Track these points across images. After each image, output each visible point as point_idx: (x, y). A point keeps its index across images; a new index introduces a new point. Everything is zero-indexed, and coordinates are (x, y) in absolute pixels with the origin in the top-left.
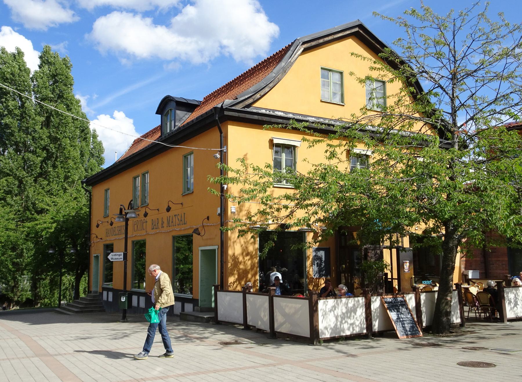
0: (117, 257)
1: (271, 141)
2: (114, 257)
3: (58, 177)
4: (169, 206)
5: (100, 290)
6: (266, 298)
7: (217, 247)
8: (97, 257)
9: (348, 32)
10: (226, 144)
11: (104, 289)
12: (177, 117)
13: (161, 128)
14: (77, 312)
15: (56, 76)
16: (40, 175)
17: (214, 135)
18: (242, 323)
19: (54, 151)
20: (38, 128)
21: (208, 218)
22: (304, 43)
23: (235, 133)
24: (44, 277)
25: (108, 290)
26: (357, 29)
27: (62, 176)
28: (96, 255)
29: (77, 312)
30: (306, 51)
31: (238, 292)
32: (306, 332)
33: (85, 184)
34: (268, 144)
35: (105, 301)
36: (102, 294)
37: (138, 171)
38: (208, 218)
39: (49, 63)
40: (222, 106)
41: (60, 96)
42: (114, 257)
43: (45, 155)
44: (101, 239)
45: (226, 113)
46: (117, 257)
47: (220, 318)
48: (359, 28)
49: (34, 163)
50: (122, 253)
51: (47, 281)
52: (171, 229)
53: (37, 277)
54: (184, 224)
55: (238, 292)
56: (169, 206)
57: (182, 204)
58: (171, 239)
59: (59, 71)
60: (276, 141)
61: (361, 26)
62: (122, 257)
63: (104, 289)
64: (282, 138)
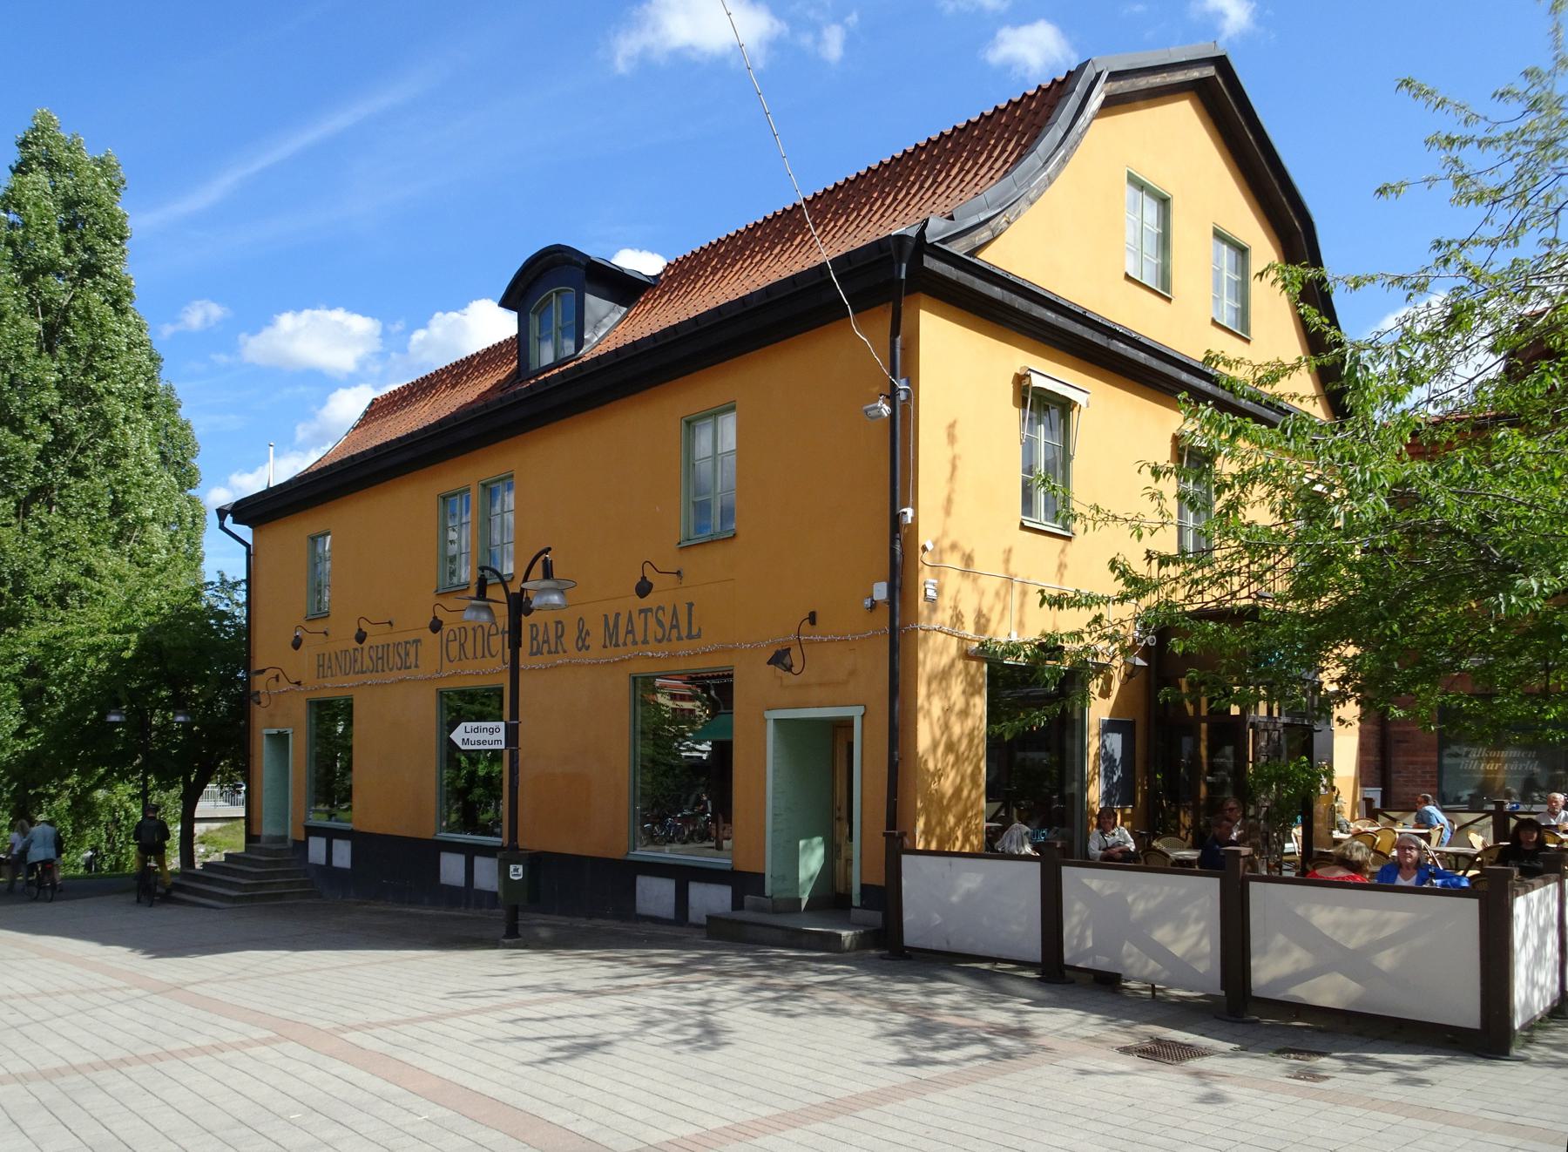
0: (485, 736)
1: (1021, 381)
2: (473, 737)
3: (93, 505)
4: (644, 578)
5: (294, 832)
6: (1205, 892)
7: (861, 710)
8: (281, 740)
9: (1179, 77)
10: (912, 377)
11: (312, 831)
12: (588, 316)
13: (519, 345)
14: (234, 899)
15: (78, 203)
16: (36, 494)
17: (863, 337)
18: (1037, 956)
19: (75, 426)
20: (29, 351)
21: (812, 618)
22: (1114, 76)
23: (941, 339)
24: (52, 791)
25: (330, 835)
26: (1210, 71)
27: (106, 502)
28: (274, 731)
29: (234, 899)
30: (1113, 104)
31: (1027, 858)
32: (1466, 1011)
33: (229, 518)
34: (1009, 390)
35: (318, 866)
36: (302, 847)
37: (467, 474)
38: (812, 618)
39: (52, 165)
40: (921, 234)
41: (89, 270)
42: (473, 737)
43: (50, 438)
44: (298, 683)
45: (930, 263)
46: (485, 736)
47: (911, 937)
48: (1219, 69)
49: (18, 459)
50: (502, 725)
51: (64, 802)
52: (622, 652)
53: (31, 792)
54: (690, 637)
55: (1027, 858)
56: (644, 578)
57: (678, 573)
58: (625, 683)
59: (85, 192)
60: (1037, 381)
61: (1221, 63)
62: (501, 736)
63: (312, 831)
64: (1053, 375)
